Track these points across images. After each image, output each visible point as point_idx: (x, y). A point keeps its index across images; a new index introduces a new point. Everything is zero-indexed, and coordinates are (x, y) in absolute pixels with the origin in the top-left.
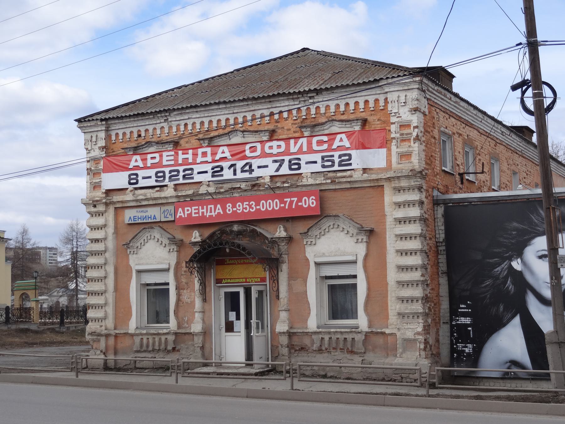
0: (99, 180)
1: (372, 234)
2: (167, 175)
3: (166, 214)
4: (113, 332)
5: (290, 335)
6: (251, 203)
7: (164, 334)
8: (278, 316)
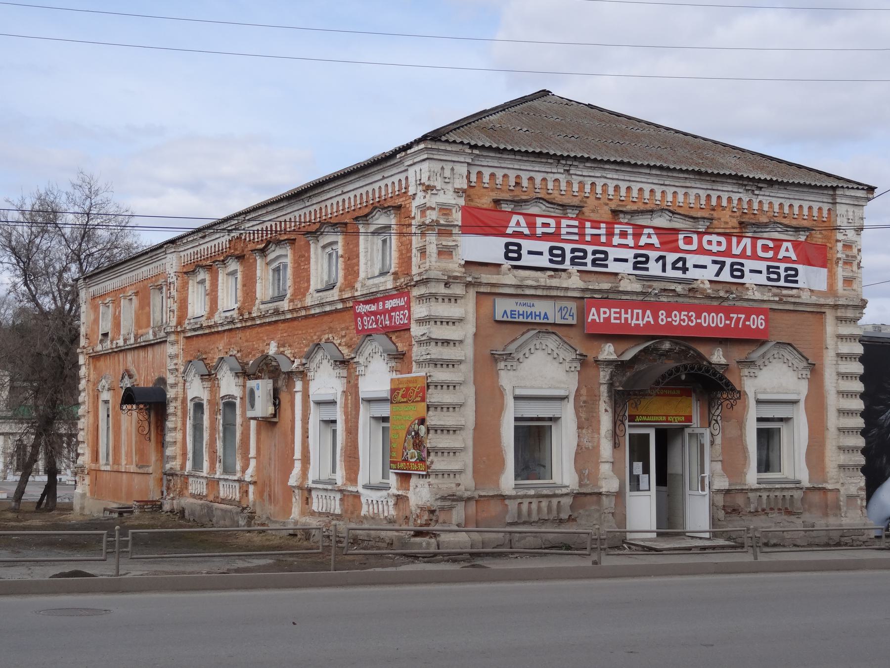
0: (454, 244)
1: (814, 370)
2: (568, 256)
3: (564, 313)
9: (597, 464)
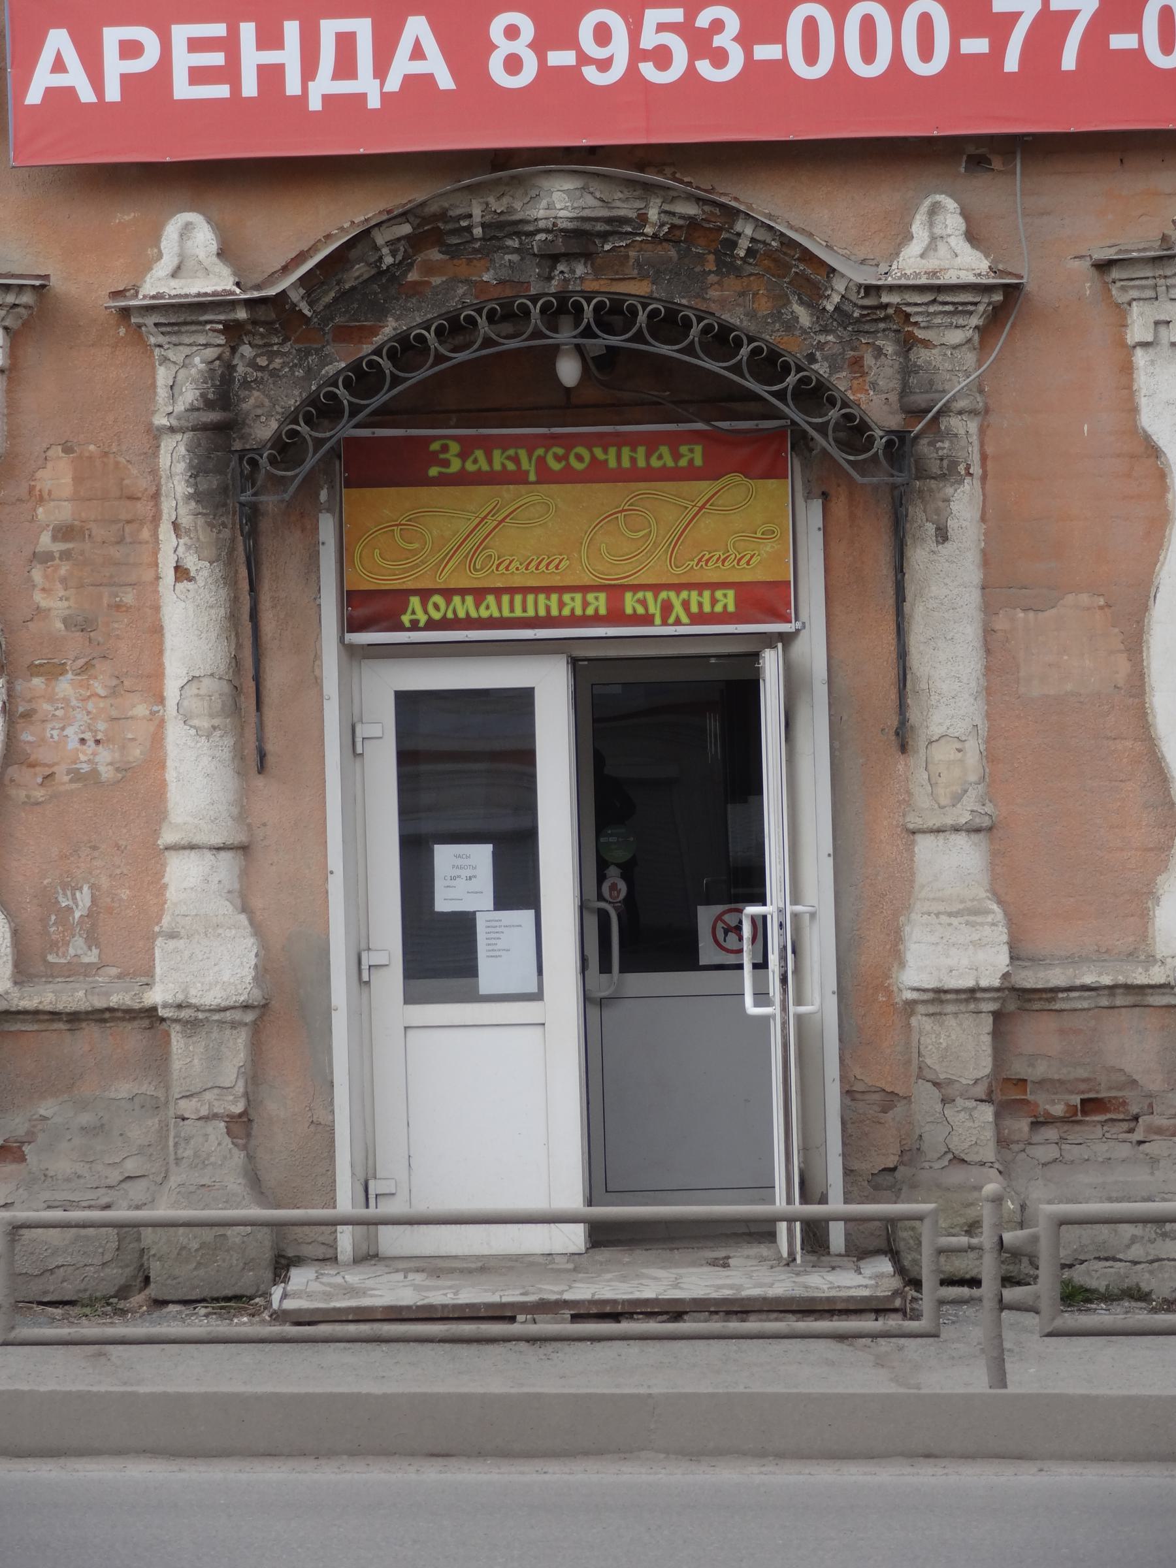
5: (1013, 1005)
6: (704, 20)
8: (904, 877)
9: (151, 858)
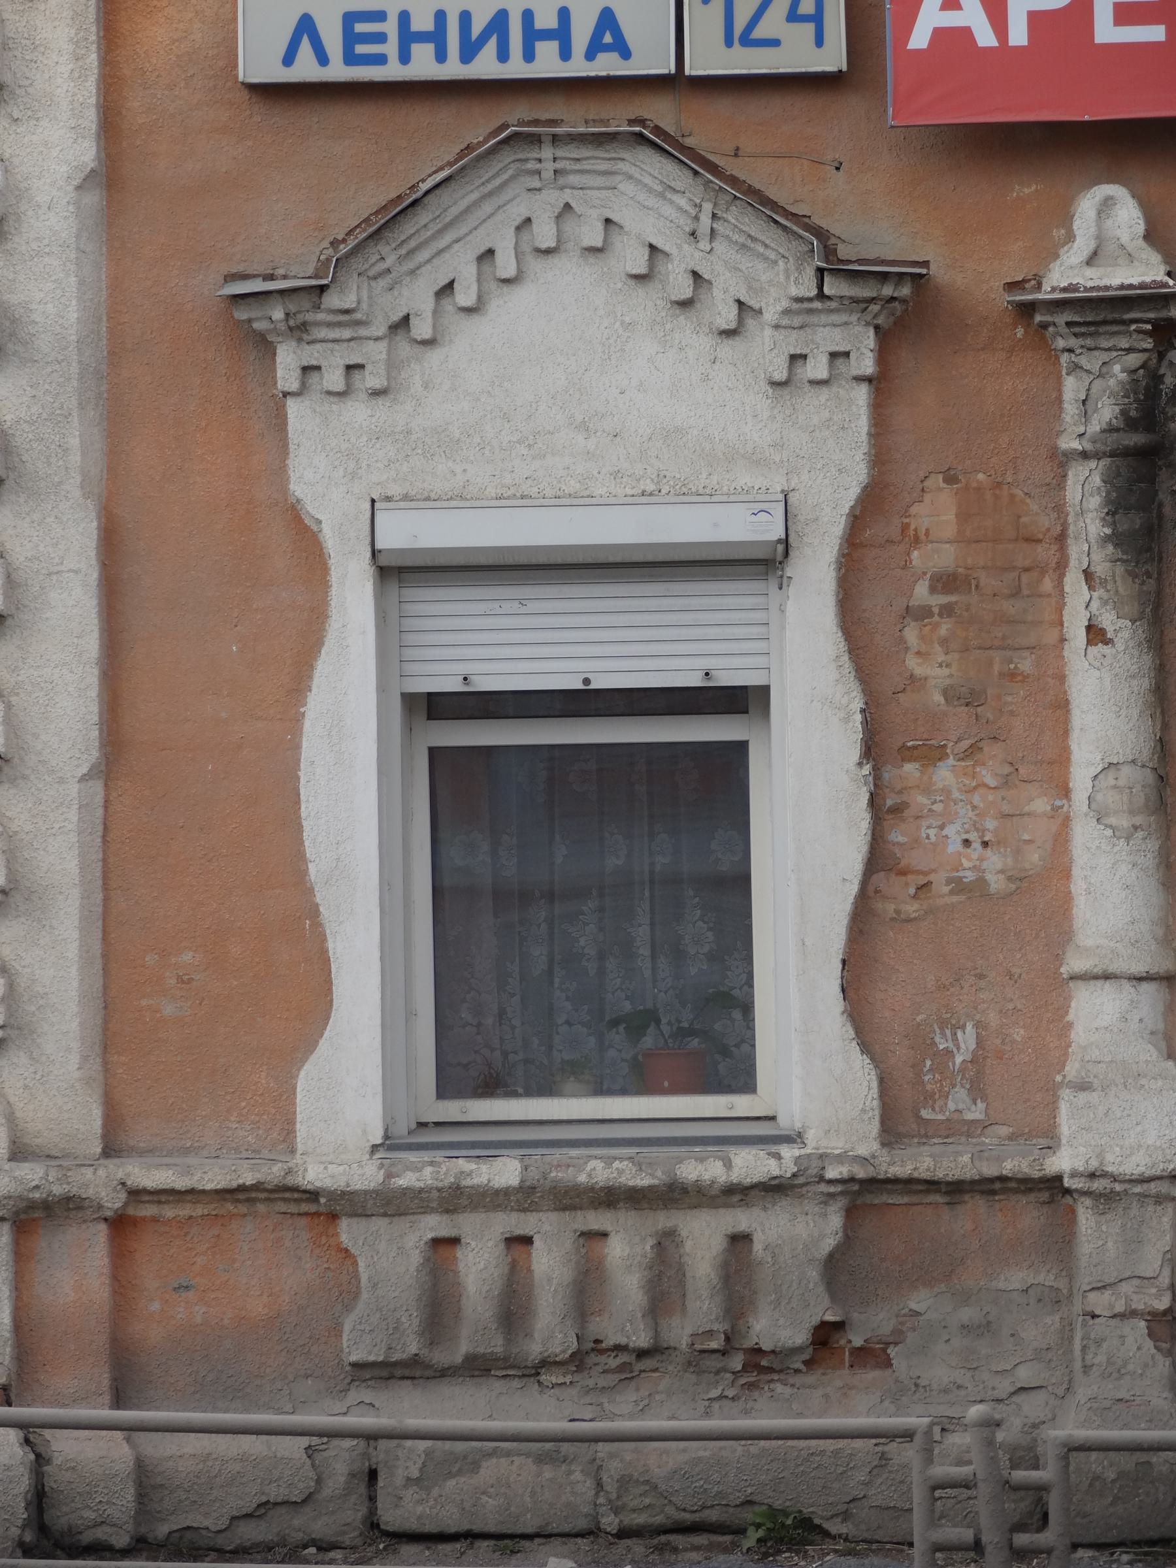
4: (102, 1183)
7: (738, 1194)
